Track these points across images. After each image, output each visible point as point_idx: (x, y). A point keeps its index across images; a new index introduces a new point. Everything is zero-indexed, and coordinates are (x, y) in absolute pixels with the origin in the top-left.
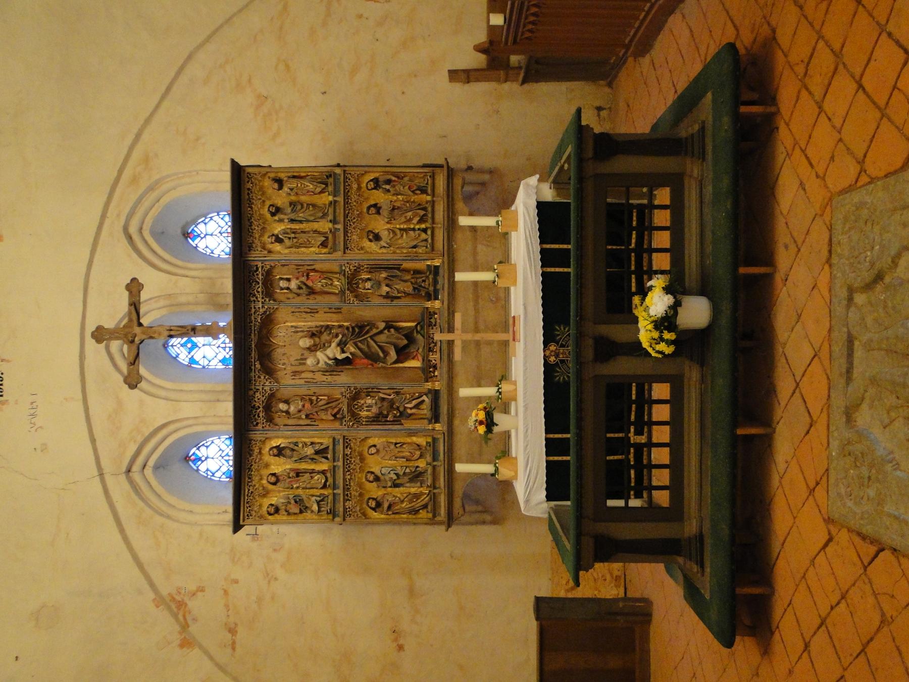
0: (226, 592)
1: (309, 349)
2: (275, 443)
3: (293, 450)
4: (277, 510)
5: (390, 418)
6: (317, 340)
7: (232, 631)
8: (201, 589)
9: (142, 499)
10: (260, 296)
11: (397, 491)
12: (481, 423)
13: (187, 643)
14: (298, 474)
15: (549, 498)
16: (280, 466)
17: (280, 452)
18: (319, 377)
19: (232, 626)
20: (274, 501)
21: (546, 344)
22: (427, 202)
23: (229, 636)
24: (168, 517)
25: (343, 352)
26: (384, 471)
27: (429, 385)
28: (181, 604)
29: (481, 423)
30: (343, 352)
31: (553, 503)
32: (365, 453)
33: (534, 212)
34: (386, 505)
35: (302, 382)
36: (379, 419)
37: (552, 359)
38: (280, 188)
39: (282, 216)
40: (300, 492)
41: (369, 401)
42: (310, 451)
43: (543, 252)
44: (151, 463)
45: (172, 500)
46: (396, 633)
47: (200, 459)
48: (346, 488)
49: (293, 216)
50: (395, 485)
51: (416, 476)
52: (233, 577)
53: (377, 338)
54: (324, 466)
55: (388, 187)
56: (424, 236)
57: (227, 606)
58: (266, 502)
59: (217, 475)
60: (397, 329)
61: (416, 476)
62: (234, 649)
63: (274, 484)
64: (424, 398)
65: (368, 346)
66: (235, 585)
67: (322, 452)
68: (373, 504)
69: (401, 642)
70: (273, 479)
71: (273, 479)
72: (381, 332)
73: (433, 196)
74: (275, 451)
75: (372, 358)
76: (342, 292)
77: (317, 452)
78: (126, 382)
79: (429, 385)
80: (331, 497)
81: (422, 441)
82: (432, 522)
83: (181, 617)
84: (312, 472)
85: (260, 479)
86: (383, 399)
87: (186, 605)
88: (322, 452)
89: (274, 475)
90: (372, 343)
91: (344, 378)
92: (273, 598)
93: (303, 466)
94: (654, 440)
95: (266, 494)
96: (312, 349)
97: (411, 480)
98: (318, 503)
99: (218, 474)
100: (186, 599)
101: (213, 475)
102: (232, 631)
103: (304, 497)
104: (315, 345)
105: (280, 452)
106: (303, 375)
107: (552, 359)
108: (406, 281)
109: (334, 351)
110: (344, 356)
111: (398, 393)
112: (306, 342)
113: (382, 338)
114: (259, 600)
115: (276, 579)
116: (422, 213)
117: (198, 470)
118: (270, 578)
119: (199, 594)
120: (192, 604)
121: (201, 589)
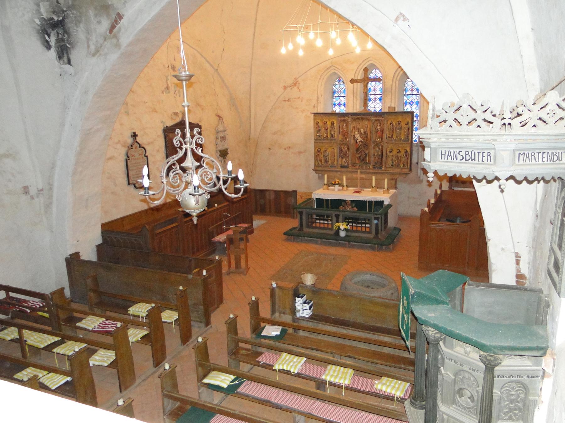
0: (299, 98)
1: (360, 132)
2: (335, 122)
3: (333, 128)
4: (317, 124)
5: (342, 154)
6: (363, 134)
7: (289, 100)
8: (300, 90)
9: (325, 71)
10: (375, 118)
11: (322, 156)
12: (335, 182)
13: (285, 88)
14: (327, 130)
15: (316, 199)
16: (329, 124)
17: (333, 124)
18: (353, 134)
19: (290, 100)
20: (320, 123)
21: (350, 200)
22: (401, 167)
23: (287, 99)
24: (320, 79)
25: (359, 142)
26: (327, 153)
27: (350, 165)
28: (295, 84)
29: (335, 182)
30: (359, 142)
31: (315, 199)
32: (332, 147)
33: (381, 200)
34: (319, 153)
35: (351, 129)
36: (341, 151)
37: (347, 202)
38: (406, 124)
39: (397, 125)
40: (322, 130)
41: (346, 149)
42: (333, 133)
43: (372, 201)
44: (336, 72)
45: (325, 79)
46: (289, 148)
47: (339, 82)
48: (323, 143)
49: (397, 128)
50: (324, 156)
51: (326, 161)
52: (303, 100)
53: (363, 152)
54: (329, 136)
55: (405, 155)
56: (390, 165)
57: (295, 98)
58: (319, 121)
59: (335, 88)
60: (366, 157)
61: (326, 161)
62: (284, 101)
63: (324, 123)
64: (347, 164)
65: (361, 149)
66: (301, 101)
67: (332, 136)
68: (319, 150)
69: (287, 149)
70: (325, 123)
71: (325, 123)
72: (364, 152)
73: (402, 168)
74: (333, 123)
75: (357, 150)
76: (375, 141)
77: (332, 135)
78: (352, 79)
79: (350, 165)
80: (320, 139)
81: (336, 162)
82: (315, 165)
83: (292, 85)
84: (327, 133)
85: (325, 119)
86: (346, 152)
87: (295, 86)
88: (332, 136)
89: (327, 123)
90: (362, 150)
91: (353, 141)
92: (298, 112)
93: (329, 130)
94: (362, 228)
95: (322, 120)
96: (360, 133)
97: (325, 160)
98: (319, 136)
99: (335, 88)
100: (297, 86)
101: (335, 86)
102: (289, 100)
103: (320, 132)
104: (362, 133)
105: (333, 124)
106: (354, 130)
107: (347, 202)
108: (378, 160)
109: (359, 139)
110: (358, 142)
111: (348, 156)
112: (362, 131)
113: (363, 153)
114: (297, 108)
115: (303, 113)
116: (397, 165)
117: (336, 81)
118: (303, 111)
119: (298, 90)
120: (296, 88)
121: (300, 90)
